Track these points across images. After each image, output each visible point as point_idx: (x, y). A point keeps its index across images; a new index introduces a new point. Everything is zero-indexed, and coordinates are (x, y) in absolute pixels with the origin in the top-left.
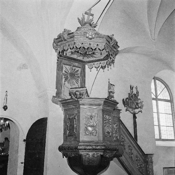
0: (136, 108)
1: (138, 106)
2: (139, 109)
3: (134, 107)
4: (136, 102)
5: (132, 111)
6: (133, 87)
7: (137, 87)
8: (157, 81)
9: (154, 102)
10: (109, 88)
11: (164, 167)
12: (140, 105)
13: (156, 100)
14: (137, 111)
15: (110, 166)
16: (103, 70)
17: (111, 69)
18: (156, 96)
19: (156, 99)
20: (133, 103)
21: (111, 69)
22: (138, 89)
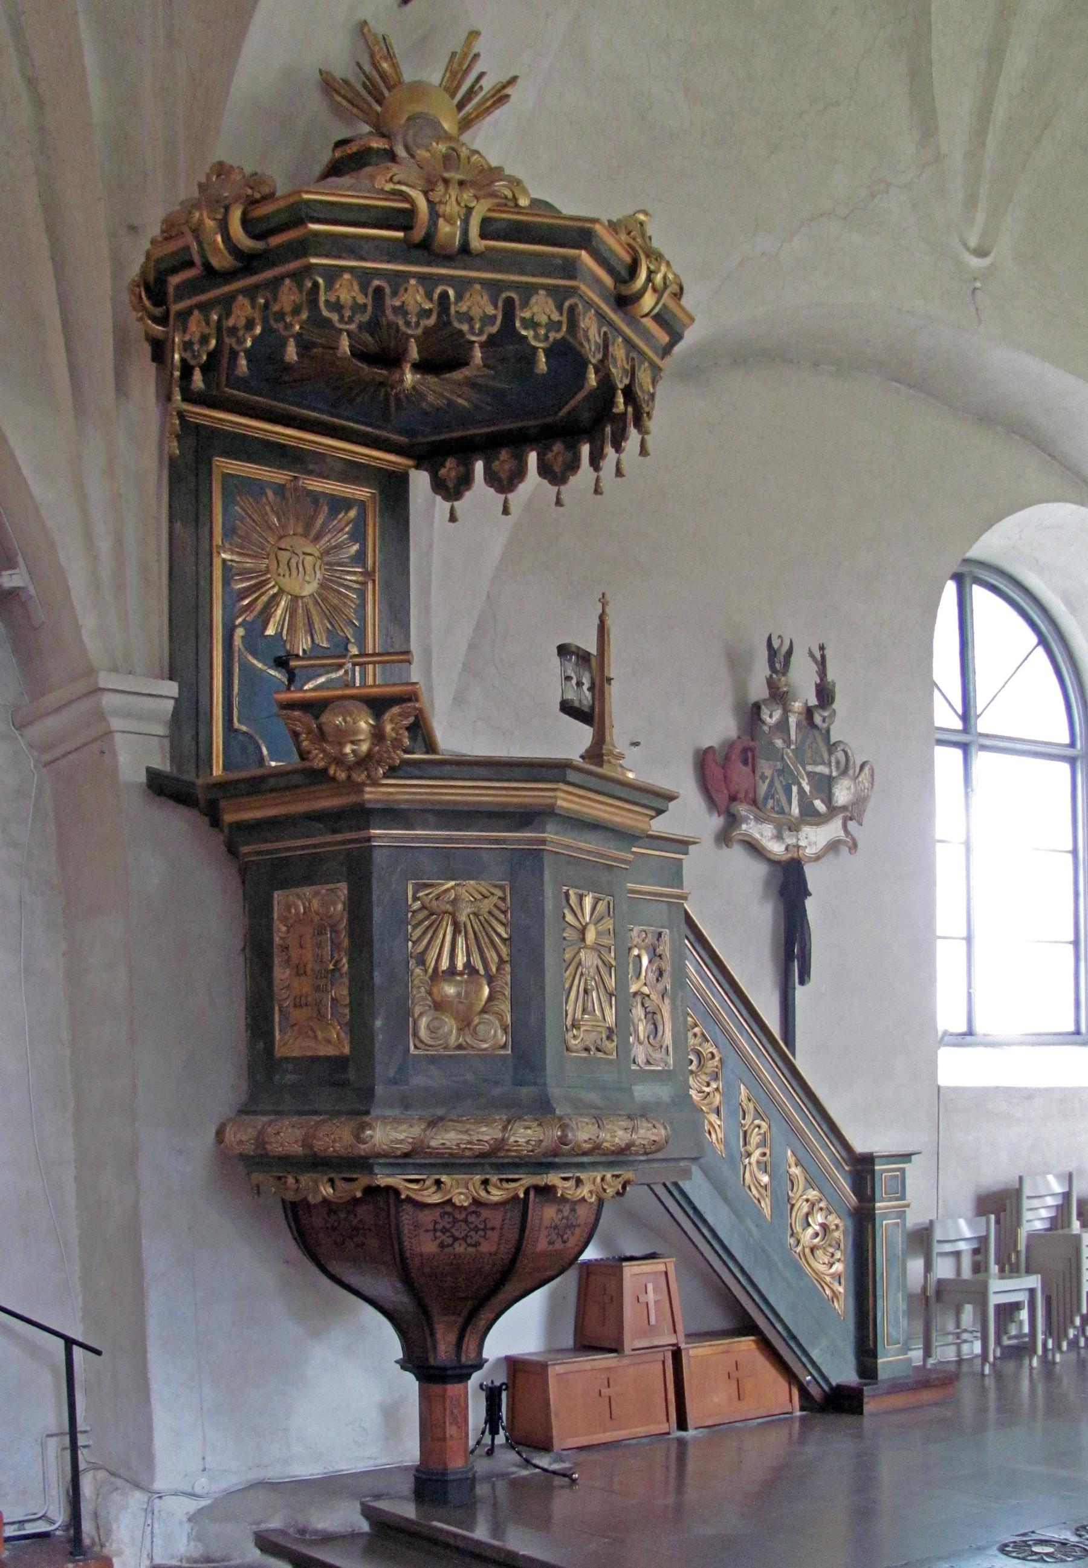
0: (810, 816)
1: (828, 800)
2: (833, 830)
3: (795, 810)
4: (809, 768)
5: (779, 837)
6: (790, 652)
7: (822, 648)
8: (980, 595)
9: (947, 759)
10: (600, 685)
11: (501, 508)
12: (842, 794)
13: (965, 747)
14: (813, 839)
15: (415, 79)
16: (501, 497)
17: (619, 473)
18: (967, 716)
19: (967, 741)
20: (788, 777)
21: (619, 473)
22: (826, 652)
